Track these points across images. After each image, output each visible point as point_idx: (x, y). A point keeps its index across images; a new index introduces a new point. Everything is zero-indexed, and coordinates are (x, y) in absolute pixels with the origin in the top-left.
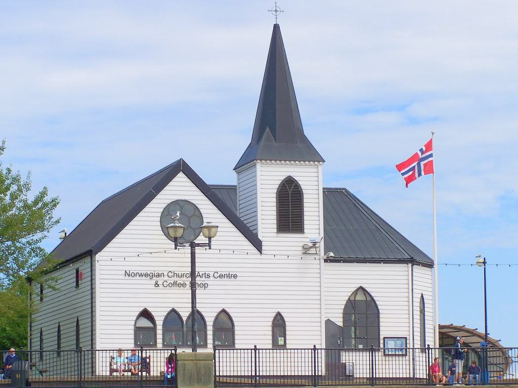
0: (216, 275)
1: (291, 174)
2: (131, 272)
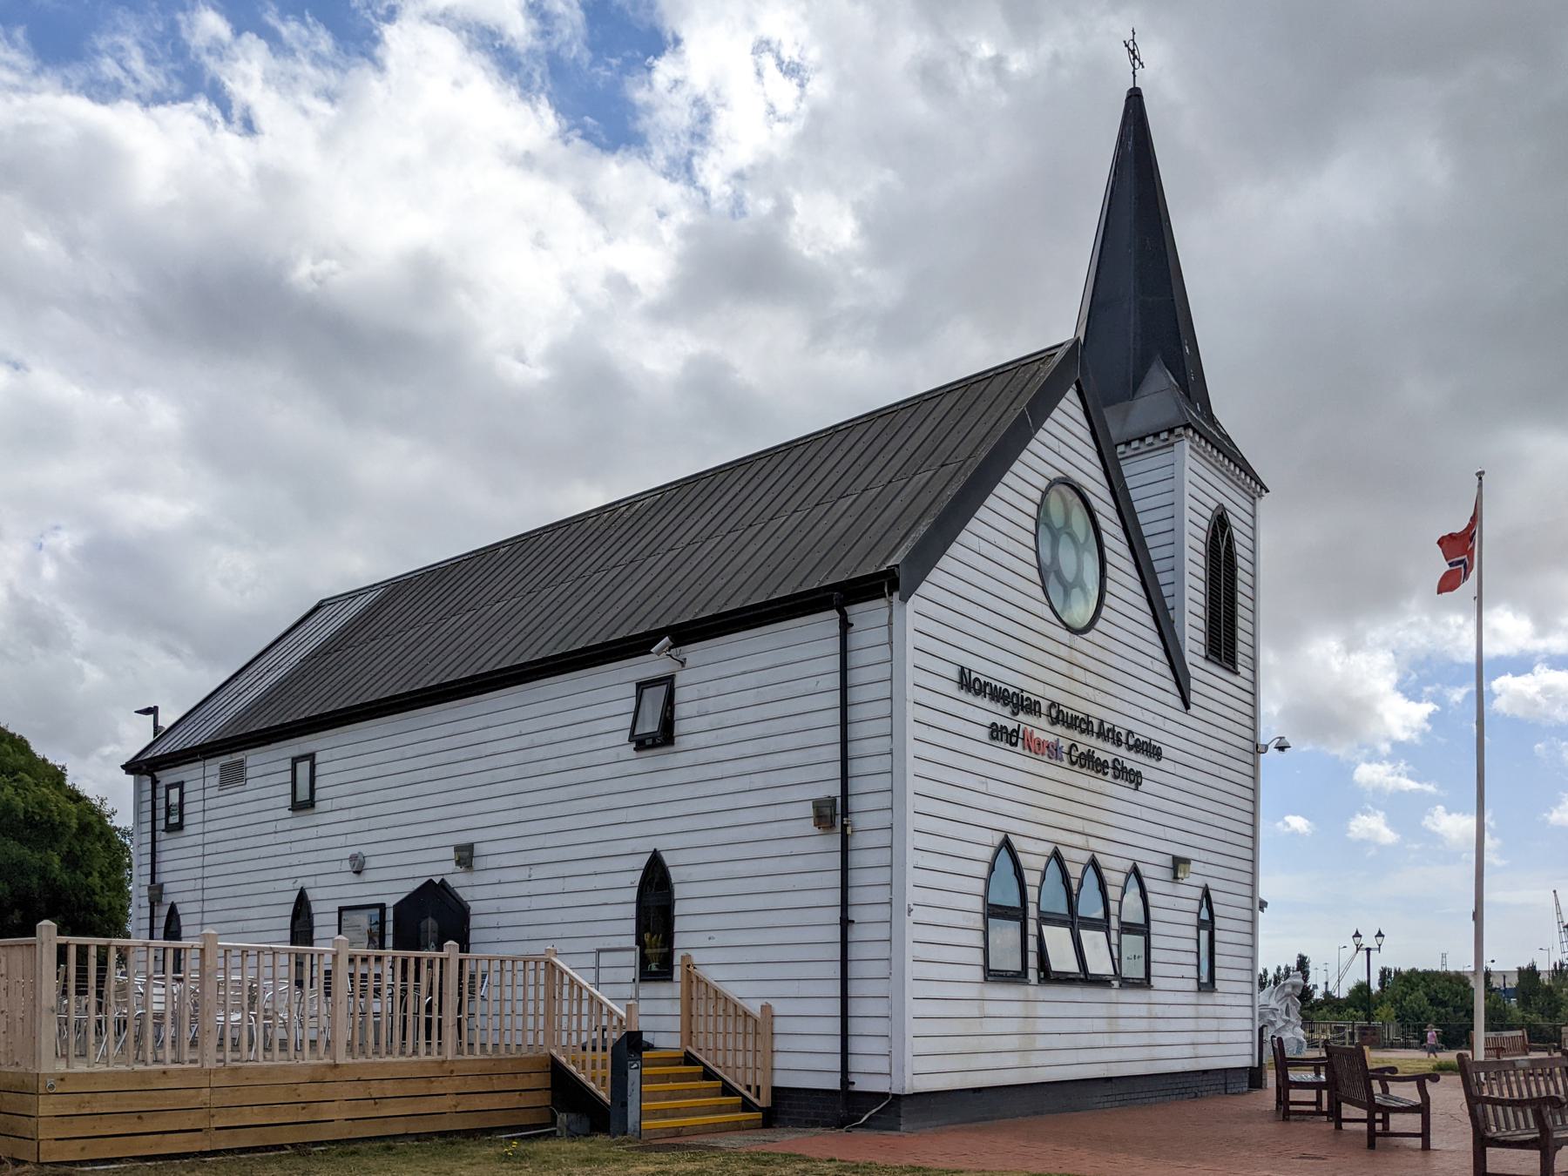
0: (1131, 742)
1: (1228, 504)
2: (974, 676)
